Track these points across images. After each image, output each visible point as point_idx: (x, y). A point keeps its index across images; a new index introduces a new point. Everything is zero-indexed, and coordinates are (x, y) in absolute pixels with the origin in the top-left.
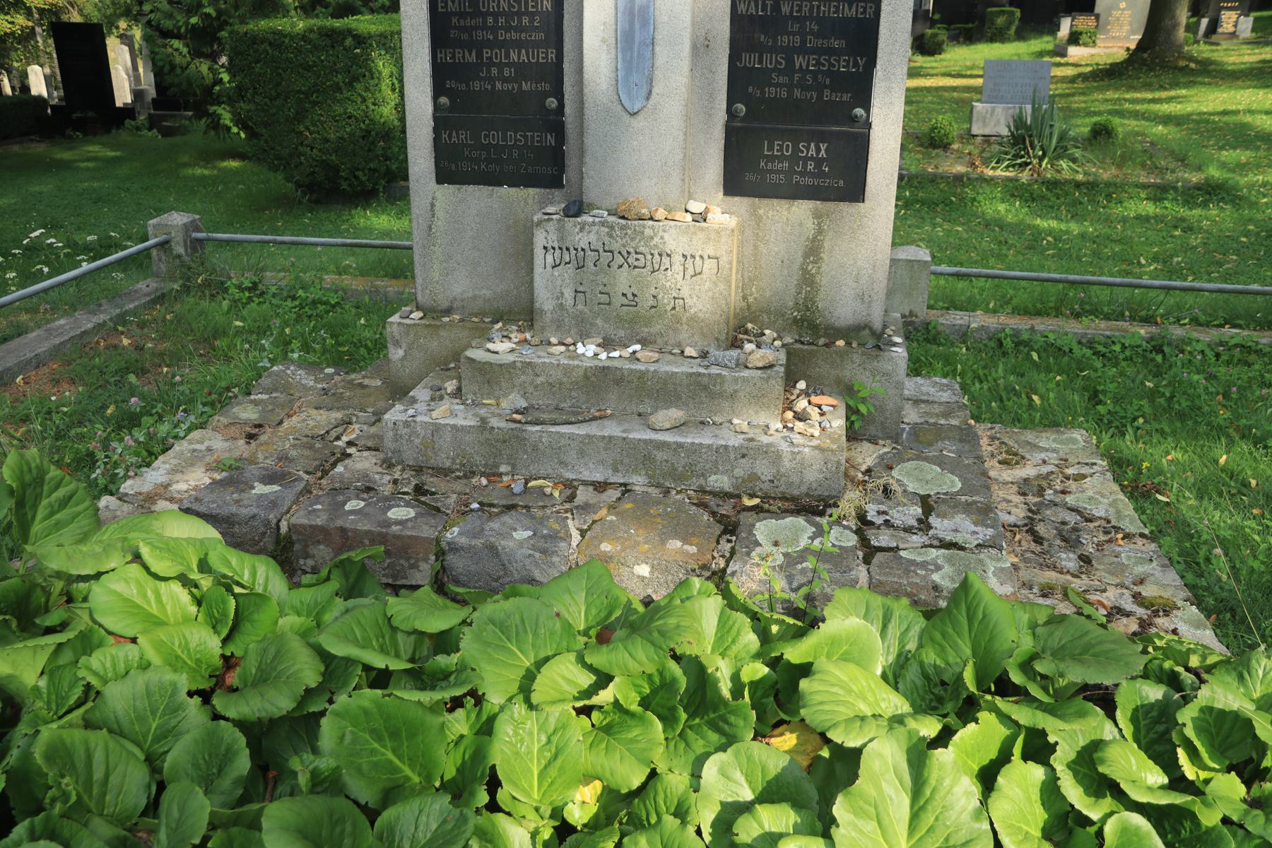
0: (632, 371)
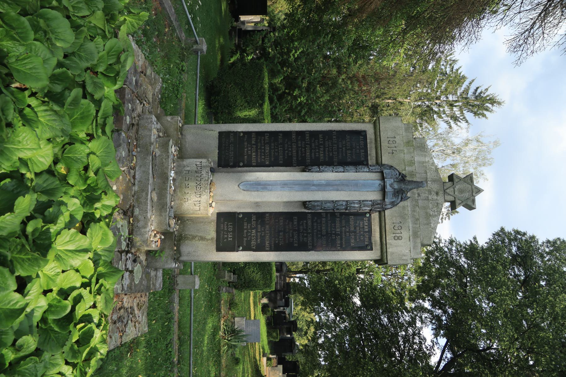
0: (167, 186)
